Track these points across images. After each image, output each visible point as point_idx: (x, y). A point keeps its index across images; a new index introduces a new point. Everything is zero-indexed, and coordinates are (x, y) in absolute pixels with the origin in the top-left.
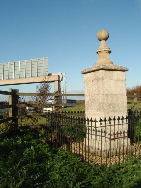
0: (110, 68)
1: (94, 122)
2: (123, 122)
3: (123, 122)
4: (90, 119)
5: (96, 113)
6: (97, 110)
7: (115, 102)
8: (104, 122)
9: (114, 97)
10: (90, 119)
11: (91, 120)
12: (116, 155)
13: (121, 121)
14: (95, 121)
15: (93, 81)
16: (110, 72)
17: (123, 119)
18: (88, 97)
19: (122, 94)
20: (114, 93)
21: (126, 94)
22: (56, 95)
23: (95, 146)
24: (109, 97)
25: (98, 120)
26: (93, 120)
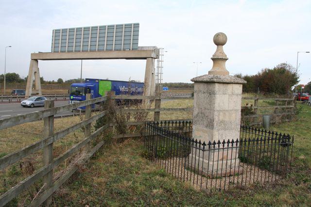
0: (225, 82)
1: (202, 145)
2: (232, 145)
3: (232, 145)
4: (198, 141)
5: (205, 129)
6: (206, 127)
7: (227, 119)
8: (213, 145)
9: (226, 113)
10: (198, 141)
11: (200, 143)
12: (213, 178)
13: (230, 145)
14: (204, 144)
15: (204, 93)
16: (225, 85)
17: (233, 142)
18: (197, 109)
19: (236, 110)
20: (227, 109)
21: (240, 110)
22: (157, 106)
23: (192, 173)
24: (221, 113)
25: (207, 143)
26: (202, 143)
